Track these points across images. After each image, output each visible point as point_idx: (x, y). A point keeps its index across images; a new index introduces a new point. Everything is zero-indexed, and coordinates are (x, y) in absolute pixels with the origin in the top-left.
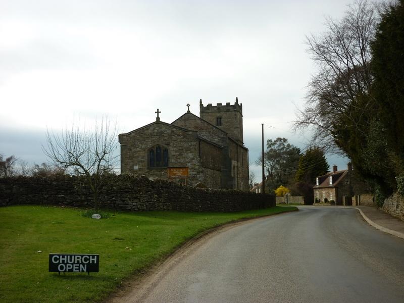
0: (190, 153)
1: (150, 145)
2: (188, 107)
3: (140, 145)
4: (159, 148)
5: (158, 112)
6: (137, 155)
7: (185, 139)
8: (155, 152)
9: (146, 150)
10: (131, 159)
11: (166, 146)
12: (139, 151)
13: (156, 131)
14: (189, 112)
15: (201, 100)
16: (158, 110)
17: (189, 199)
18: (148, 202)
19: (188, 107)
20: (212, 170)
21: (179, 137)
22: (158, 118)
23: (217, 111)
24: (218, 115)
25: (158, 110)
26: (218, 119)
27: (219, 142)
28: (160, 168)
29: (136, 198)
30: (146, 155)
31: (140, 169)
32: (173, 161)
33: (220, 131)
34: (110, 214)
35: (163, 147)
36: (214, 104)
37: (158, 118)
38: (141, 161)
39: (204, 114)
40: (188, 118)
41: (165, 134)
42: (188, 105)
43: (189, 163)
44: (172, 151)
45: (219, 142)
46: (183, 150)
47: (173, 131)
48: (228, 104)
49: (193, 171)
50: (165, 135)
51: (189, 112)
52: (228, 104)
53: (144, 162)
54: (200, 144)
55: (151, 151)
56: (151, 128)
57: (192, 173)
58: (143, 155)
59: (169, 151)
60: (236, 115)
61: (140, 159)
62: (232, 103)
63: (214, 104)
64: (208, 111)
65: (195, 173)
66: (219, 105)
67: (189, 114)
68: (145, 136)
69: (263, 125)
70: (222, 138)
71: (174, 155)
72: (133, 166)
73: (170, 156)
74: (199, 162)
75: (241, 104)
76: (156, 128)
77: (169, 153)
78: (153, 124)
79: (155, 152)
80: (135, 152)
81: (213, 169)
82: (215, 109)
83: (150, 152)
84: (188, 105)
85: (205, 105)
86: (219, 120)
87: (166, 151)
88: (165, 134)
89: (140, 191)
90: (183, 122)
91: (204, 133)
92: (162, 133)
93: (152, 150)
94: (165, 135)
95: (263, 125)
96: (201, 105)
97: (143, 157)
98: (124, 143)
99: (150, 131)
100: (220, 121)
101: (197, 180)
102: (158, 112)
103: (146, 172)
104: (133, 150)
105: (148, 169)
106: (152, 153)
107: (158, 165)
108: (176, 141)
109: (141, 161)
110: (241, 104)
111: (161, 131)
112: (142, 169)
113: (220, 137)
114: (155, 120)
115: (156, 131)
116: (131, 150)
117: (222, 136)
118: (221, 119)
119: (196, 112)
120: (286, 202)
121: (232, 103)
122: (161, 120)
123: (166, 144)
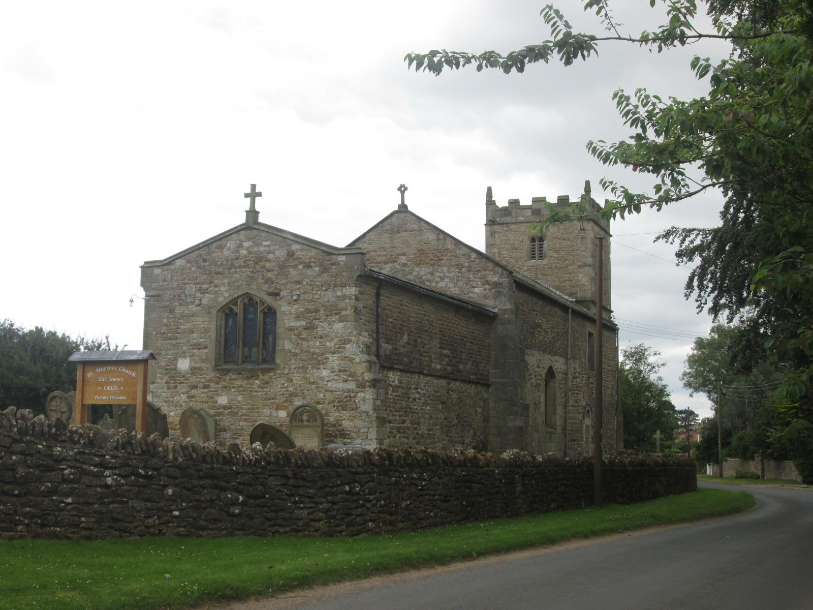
0: (340, 321)
1: (225, 295)
2: (403, 193)
3: (198, 295)
4: (250, 302)
5: (253, 194)
6: (188, 326)
7: (325, 277)
8: (240, 316)
9: (214, 311)
10: (170, 339)
11: (269, 300)
12: (194, 314)
13: (245, 252)
14: (403, 208)
15: (489, 189)
17: (107, 486)
19: (403, 193)
20: (443, 382)
21: (309, 272)
22: (252, 214)
23: (533, 218)
26: (533, 240)
27: (486, 297)
28: (249, 366)
30: (213, 326)
31: (194, 370)
32: (288, 345)
33: (490, 265)
34: (559, 455)
36: (526, 201)
37: (252, 214)
38: (199, 347)
39: (497, 228)
41: (269, 261)
42: (403, 189)
43: (333, 353)
44: (288, 316)
45: (486, 297)
46: (317, 311)
47: (291, 254)
48: (563, 200)
49: (346, 381)
51: (403, 208)
53: (206, 348)
54: (378, 295)
55: (227, 312)
56: (231, 244)
57: (341, 385)
58: (204, 327)
59: (278, 316)
60: (583, 229)
61: (195, 337)
62: (575, 198)
63: (526, 201)
64: (509, 219)
65: (352, 385)
67: (403, 215)
68: (213, 268)
70: (496, 285)
71: (291, 329)
72: (176, 359)
73: (280, 330)
76: (246, 244)
77: (279, 324)
78: (328, 251)
80: (183, 316)
82: (528, 213)
83: (227, 316)
84: (403, 189)
86: (537, 243)
87: (270, 312)
88: (269, 261)
90: (385, 238)
92: (259, 259)
93: (232, 310)
94: (268, 265)
96: (490, 202)
98: (155, 289)
99: (226, 252)
100: (541, 247)
101: (356, 409)
102: (253, 194)
103: (210, 381)
104: (179, 310)
105: (216, 367)
107: (246, 359)
108: (299, 282)
109: (199, 347)
111: (257, 252)
112: (199, 369)
113: (487, 283)
115: (245, 252)
116: (172, 311)
117: (496, 279)
120: (759, 473)
122: (262, 219)
123: (269, 294)
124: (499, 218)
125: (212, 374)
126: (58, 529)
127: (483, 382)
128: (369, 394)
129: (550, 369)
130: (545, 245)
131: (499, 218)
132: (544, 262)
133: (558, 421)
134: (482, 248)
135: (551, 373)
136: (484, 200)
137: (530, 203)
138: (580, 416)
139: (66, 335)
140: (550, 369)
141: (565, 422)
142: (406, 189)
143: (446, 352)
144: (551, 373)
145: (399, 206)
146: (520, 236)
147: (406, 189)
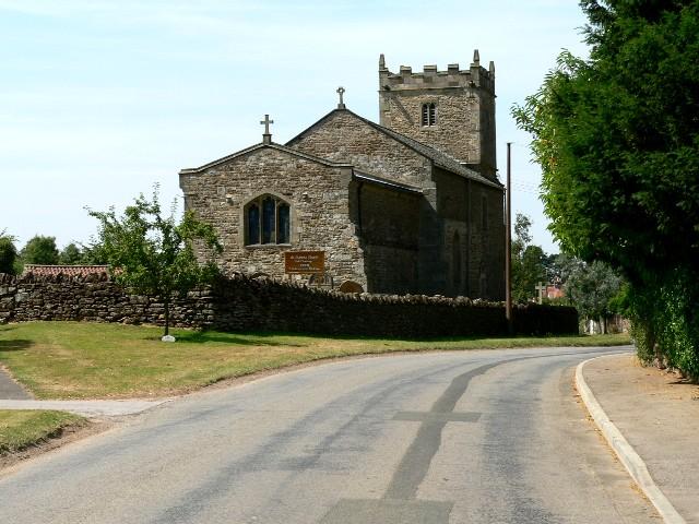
1: (250, 196)
2: (341, 95)
8: (260, 208)
15: (382, 56)
16: (267, 116)
18: (246, 316)
19: (341, 95)
20: (392, 250)
22: (267, 136)
24: (428, 97)
25: (267, 116)
26: (425, 106)
29: (227, 310)
35: (279, 200)
36: (418, 69)
37: (267, 136)
40: (152, 375)
42: (341, 91)
44: (297, 211)
50: (282, 173)
52: (453, 69)
55: (251, 209)
62: (465, 66)
63: (418, 69)
65: (349, 257)
66: (431, 70)
69: (509, 145)
74: (359, 233)
75: (492, 63)
79: (260, 208)
81: (398, 245)
84: (341, 91)
85: (395, 70)
87: (285, 208)
89: (233, 299)
91: (379, 157)
95: (509, 145)
96: (383, 71)
97: (235, 222)
102: (267, 122)
106: (253, 213)
110: (492, 63)
114: (261, 140)
118: (433, 106)
119: (367, 104)
121: (465, 66)
124: (393, 85)
125: (242, 251)
126: (656, 345)
127: (414, 247)
128: (361, 262)
129: (457, 231)
130: (436, 111)
131: (393, 85)
132: (435, 127)
133: (463, 278)
134: (376, 120)
135: (457, 236)
136: (377, 68)
137: (422, 71)
138: (477, 271)
139: (121, 217)
140: (457, 231)
141: (467, 277)
142: (344, 91)
143: (393, 227)
144: (457, 236)
145: (339, 105)
146: (414, 105)
147: (344, 91)
